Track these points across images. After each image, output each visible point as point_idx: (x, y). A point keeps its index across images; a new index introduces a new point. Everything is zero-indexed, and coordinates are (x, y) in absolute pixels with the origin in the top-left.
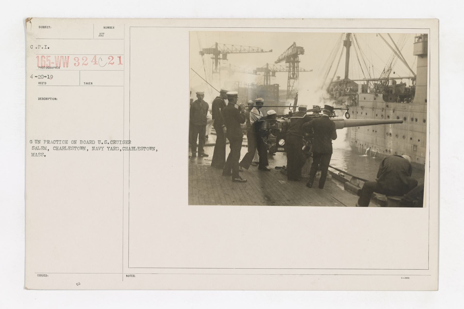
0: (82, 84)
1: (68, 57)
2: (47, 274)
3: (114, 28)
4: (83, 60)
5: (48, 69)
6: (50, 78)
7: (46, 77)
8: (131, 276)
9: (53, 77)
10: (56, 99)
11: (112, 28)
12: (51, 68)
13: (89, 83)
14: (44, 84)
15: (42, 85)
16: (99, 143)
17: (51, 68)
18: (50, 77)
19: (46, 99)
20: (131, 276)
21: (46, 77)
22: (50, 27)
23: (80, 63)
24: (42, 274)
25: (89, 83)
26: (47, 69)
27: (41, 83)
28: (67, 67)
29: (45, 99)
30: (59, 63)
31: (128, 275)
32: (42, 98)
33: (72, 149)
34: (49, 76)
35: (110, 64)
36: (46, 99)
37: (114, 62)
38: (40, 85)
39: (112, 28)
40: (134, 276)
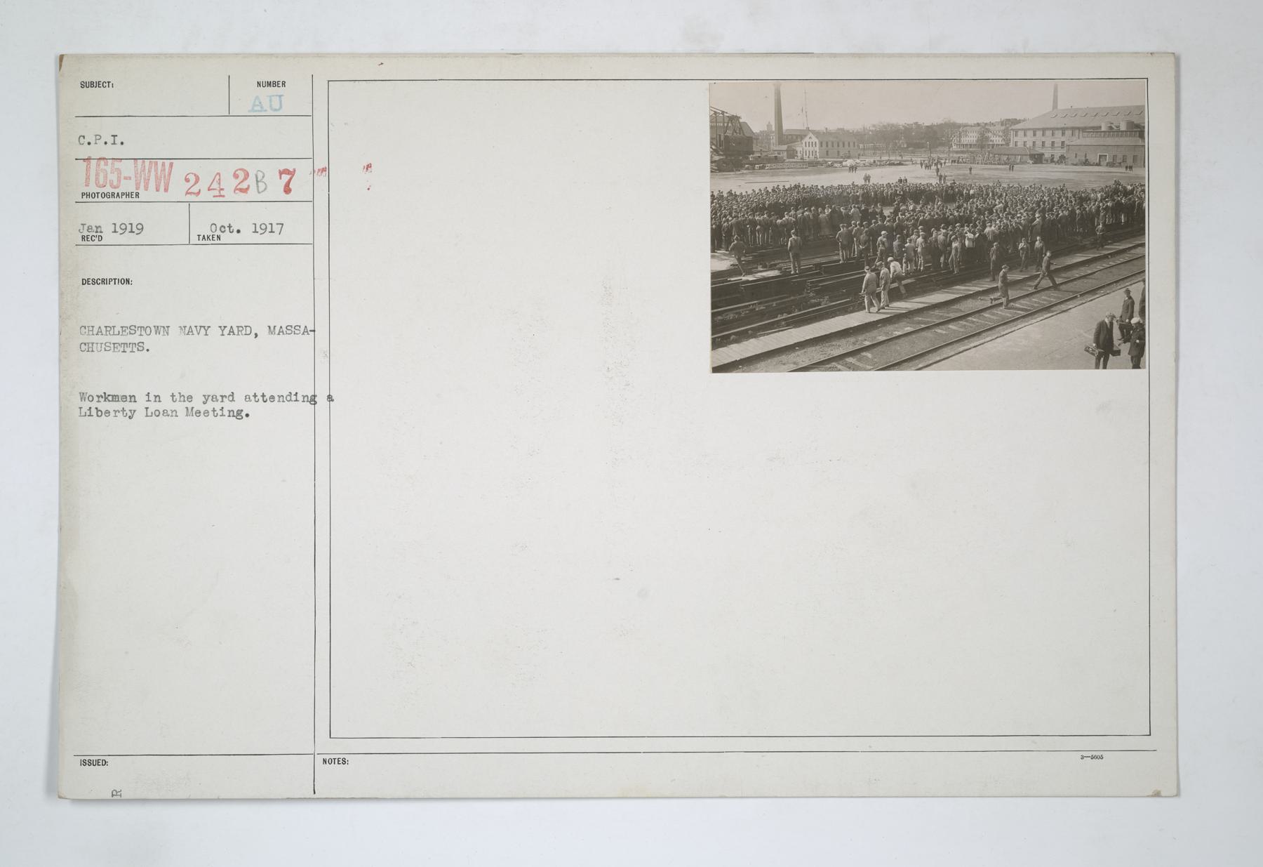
0: (194, 240)
1: (171, 165)
2: (107, 759)
3: (284, 84)
4: (187, 180)
5: (109, 200)
6: (137, 231)
7: (130, 178)
8: (336, 761)
9: (142, 228)
10: (128, 281)
11: (281, 85)
12: (116, 195)
13: (211, 238)
14: (96, 242)
15: (91, 243)
17: (116, 195)
18: (134, 229)
19: (104, 281)
20: (336, 761)
21: (130, 178)
22: (110, 84)
23: (200, 178)
24: (92, 758)
25: (211, 238)
26: (103, 200)
27: (90, 239)
28: (166, 190)
29: (99, 282)
30: (145, 179)
31: (327, 757)
32: (91, 280)
33: (135, 327)
34: (255, 227)
35: (237, 191)
36: (104, 281)
37: (249, 186)
38: (86, 243)
39: (281, 85)
40: (344, 762)
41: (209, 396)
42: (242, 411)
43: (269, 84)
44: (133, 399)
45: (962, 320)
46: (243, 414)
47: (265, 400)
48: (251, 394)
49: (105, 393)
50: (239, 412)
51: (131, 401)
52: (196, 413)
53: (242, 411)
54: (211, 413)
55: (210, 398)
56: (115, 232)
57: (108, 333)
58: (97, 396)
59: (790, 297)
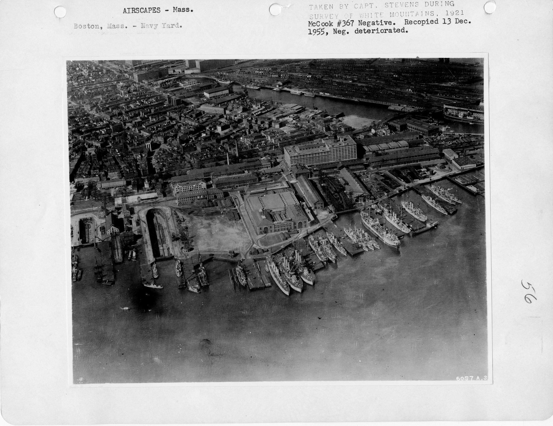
16: (432, 5)
41: (387, 22)
42: (345, 30)
43: (134, 10)
44: (97, 27)
45: (91, 213)
46: (346, 32)
47: (378, 24)
48: (375, 21)
49: (330, 21)
50: (344, 31)
51: (96, 28)
52: (338, 32)
53: (345, 30)
54: (87, 26)
55: (388, 22)
56: (310, 34)
57: (133, 11)
58: (372, 30)
59: (352, 96)
